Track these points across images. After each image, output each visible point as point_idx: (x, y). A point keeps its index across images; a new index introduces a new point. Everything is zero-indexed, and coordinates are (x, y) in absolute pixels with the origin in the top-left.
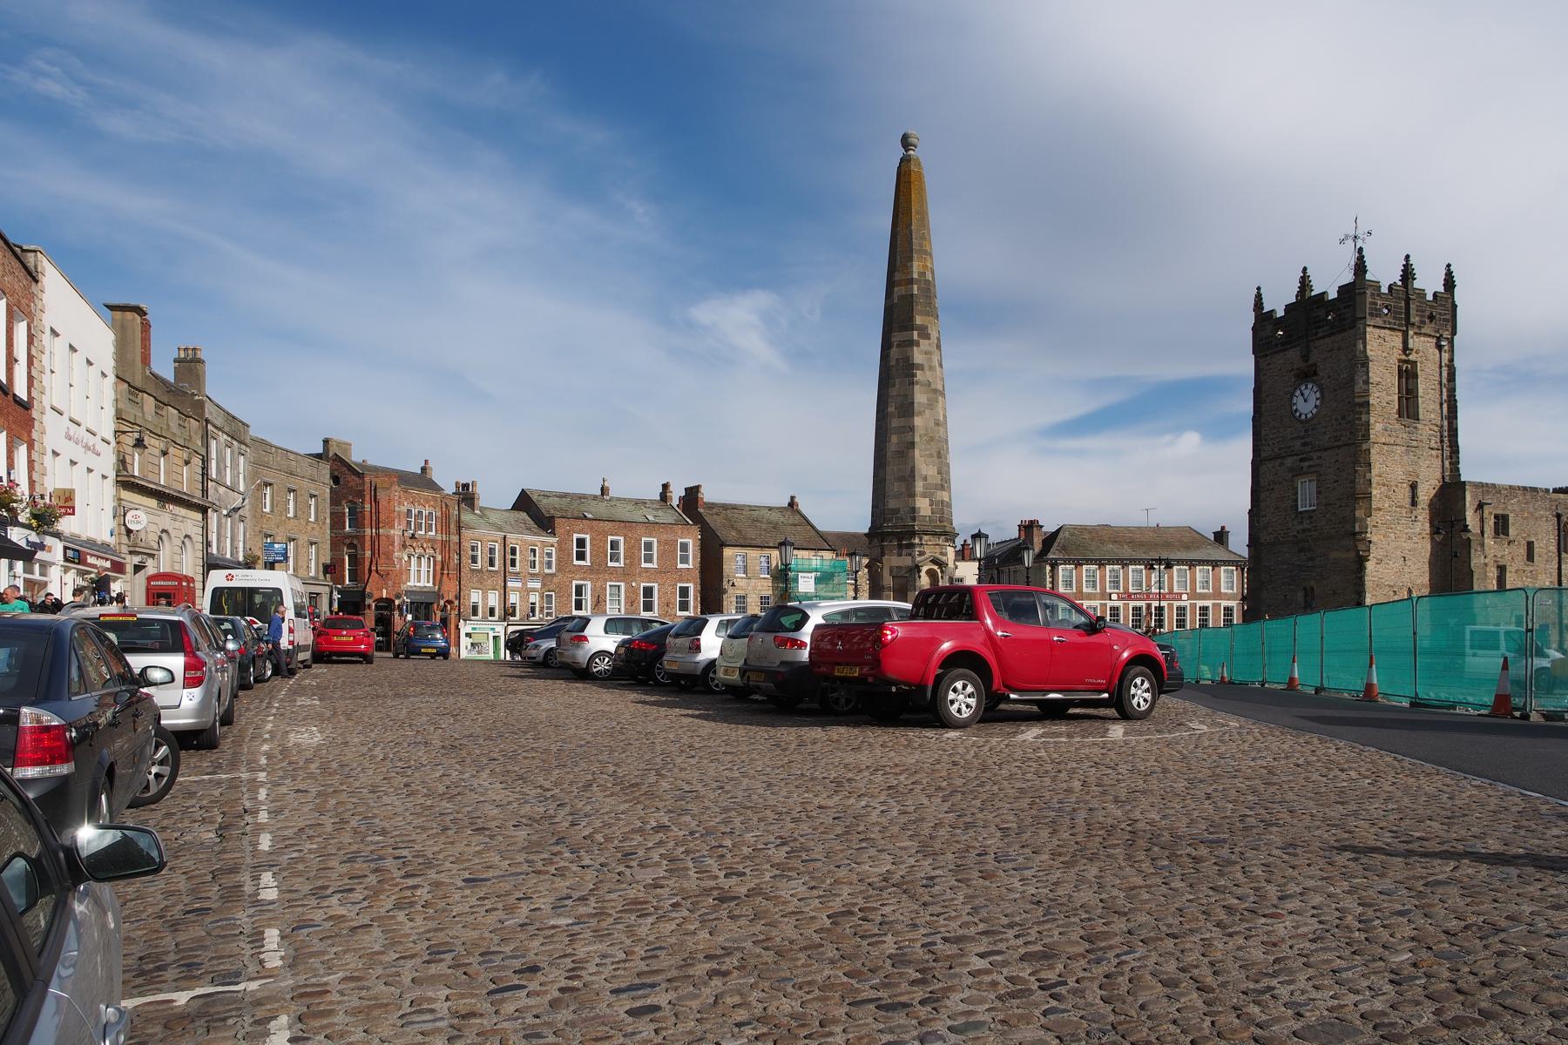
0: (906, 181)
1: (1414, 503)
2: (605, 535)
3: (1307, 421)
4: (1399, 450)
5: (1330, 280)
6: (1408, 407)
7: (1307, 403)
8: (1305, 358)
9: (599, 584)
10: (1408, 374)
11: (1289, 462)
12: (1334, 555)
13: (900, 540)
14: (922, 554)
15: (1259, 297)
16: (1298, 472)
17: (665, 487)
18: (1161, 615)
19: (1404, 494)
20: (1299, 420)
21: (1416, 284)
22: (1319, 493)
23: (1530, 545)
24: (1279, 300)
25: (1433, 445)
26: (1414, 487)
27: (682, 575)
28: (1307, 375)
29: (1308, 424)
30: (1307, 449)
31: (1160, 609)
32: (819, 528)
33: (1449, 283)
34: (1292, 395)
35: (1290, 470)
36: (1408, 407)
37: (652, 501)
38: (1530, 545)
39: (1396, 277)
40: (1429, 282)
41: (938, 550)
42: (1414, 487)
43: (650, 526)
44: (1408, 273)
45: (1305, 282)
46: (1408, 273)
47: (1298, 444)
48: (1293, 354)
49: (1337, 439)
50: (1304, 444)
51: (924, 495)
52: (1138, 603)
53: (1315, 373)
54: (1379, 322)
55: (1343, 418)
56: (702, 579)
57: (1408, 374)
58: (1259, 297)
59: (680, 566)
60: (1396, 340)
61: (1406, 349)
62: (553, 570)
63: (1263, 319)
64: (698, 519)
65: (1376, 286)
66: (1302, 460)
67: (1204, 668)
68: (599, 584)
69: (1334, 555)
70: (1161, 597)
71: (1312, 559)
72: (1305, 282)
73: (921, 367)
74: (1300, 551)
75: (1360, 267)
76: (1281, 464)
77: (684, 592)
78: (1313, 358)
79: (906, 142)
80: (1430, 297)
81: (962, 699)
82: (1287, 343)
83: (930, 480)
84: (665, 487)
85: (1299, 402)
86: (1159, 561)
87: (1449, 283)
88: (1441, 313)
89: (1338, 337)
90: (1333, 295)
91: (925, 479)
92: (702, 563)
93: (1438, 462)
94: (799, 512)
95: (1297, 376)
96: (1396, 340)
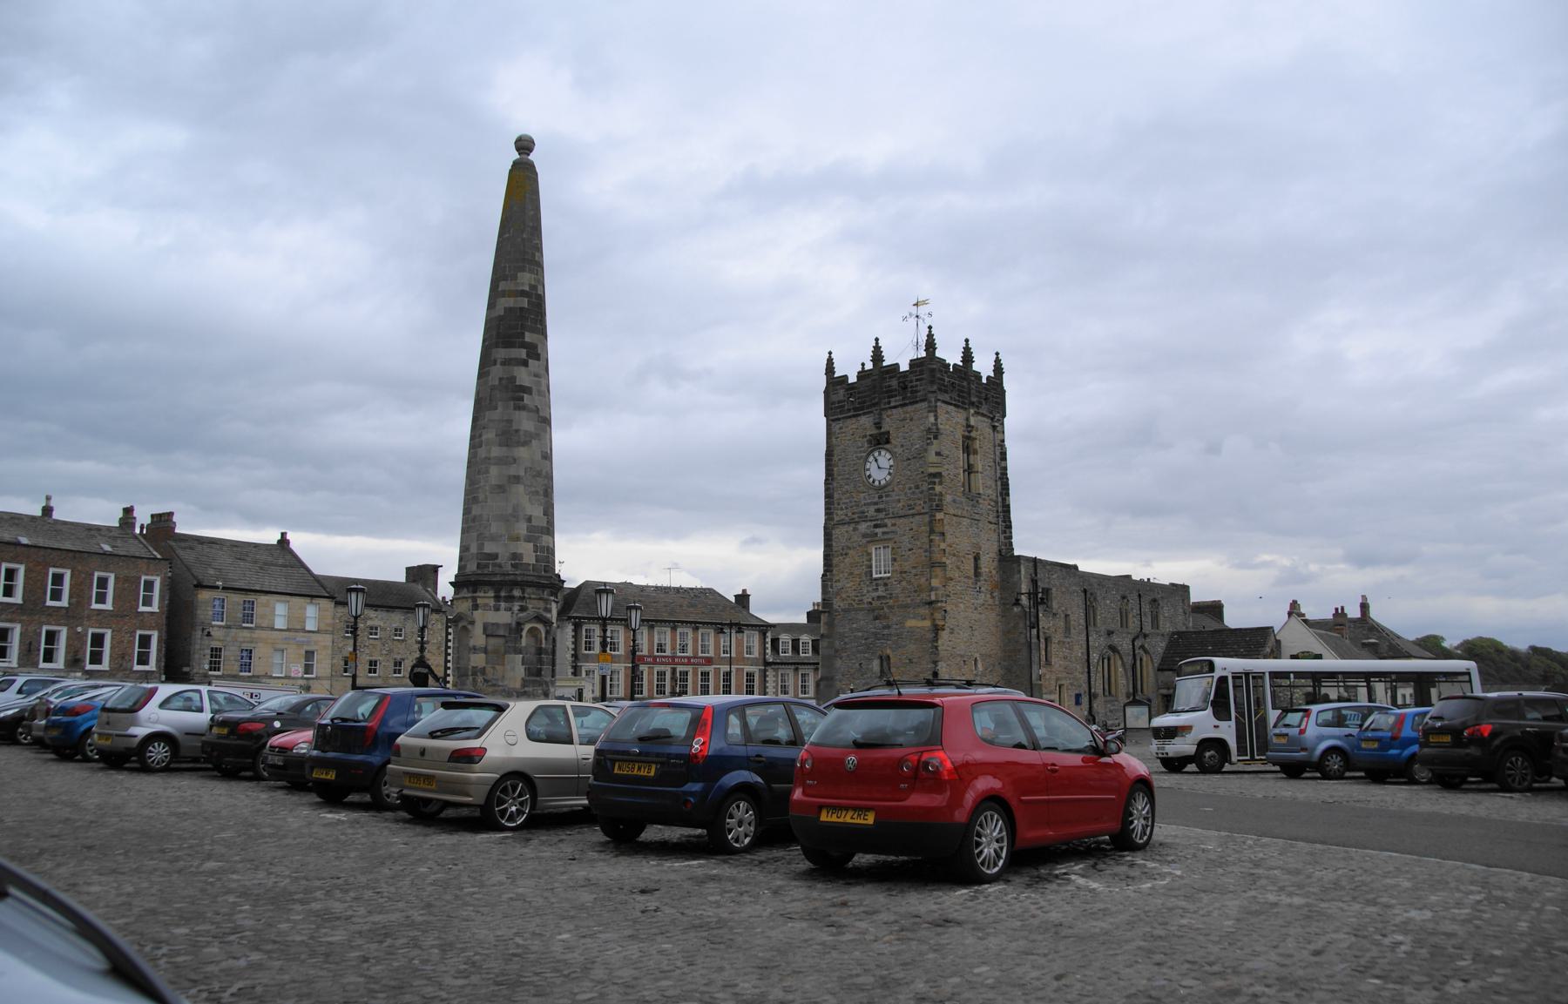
0: (523, 183)
1: (977, 574)
2: (47, 566)
3: (881, 488)
4: (966, 522)
5: (901, 355)
7: (880, 468)
8: (878, 425)
9: (32, 628)
11: (863, 527)
12: (910, 623)
13: (497, 591)
14: (523, 609)
15: (830, 362)
16: (872, 538)
18: (804, 687)
19: (969, 566)
22: (894, 560)
24: (849, 369)
25: (991, 518)
26: (977, 558)
28: (880, 440)
29: (882, 490)
30: (882, 515)
31: (728, 675)
32: (316, 571)
33: (998, 369)
34: (866, 460)
35: (865, 536)
37: (109, 529)
40: (983, 366)
41: (541, 604)
42: (977, 558)
43: (107, 559)
44: (968, 356)
45: (877, 355)
46: (968, 356)
47: (871, 511)
48: (866, 421)
49: (911, 507)
50: (878, 511)
51: (528, 540)
52: (662, 668)
53: (888, 442)
54: (946, 397)
55: (917, 487)
56: (168, 625)
58: (830, 362)
59: (142, 609)
63: (834, 383)
64: (169, 559)
65: (978, 375)
66: (876, 526)
68: (32, 628)
69: (910, 623)
70: (709, 661)
71: (888, 627)
72: (877, 355)
73: (528, 390)
74: (876, 618)
75: (931, 345)
76: (855, 529)
77: (145, 641)
81: (991, 841)
82: (858, 410)
83: (534, 523)
84: (128, 511)
85: (872, 467)
86: (731, 625)
87: (998, 369)
89: (910, 408)
90: (904, 367)
91: (529, 519)
93: (995, 536)
94: (292, 553)
95: (869, 442)
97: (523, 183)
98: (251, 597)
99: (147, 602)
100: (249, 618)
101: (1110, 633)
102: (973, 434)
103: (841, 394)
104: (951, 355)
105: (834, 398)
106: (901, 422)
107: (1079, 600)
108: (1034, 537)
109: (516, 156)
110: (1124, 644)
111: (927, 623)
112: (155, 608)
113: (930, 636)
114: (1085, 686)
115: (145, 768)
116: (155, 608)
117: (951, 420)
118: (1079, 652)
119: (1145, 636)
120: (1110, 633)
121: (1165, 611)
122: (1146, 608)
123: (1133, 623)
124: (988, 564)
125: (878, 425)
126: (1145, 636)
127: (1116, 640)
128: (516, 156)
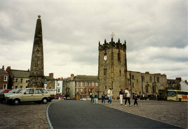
0: (39, 22)
3: (106, 61)
6: (119, 58)
8: (105, 52)
10: (119, 54)
17: (3, 66)
20: (104, 61)
21: (120, 43)
23: (137, 80)
24: (102, 43)
26: (120, 72)
27: (5, 82)
28: (105, 54)
29: (106, 61)
33: (125, 43)
36: (119, 58)
38: (137, 80)
39: (117, 42)
40: (122, 42)
44: (119, 41)
46: (119, 41)
48: (104, 51)
57: (119, 54)
59: (4, 81)
60: (118, 50)
61: (119, 51)
62: (5, 76)
65: (121, 44)
67: (109, 91)
74: (105, 80)
78: (106, 52)
79: (39, 17)
80: (122, 44)
82: (103, 50)
84: (3, 66)
87: (125, 43)
88: (124, 47)
92: (9, 80)
96: (118, 50)
97: (39, 22)
98: (18, 78)
99: (5, 80)
100: (21, 82)
101: (147, 83)
102: (120, 53)
103: (101, 48)
104: (116, 41)
105: (100, 48)
106: (109, 52)
107: (141, 77)
108: (131, 67)
109: (38, 18)
110: (151, 84)
111: (111, 81)
112: (6, 81)
113: (111, 83)
114: (142, 91)
115: (43, 103)
116: (6, 81)
117: (116, 51)
118: (140, 85)
119: (156, 83)
120: (147, 83)
121: (160, 79)
122: (156, 79)
123: (153, 81)
124: (123, 72)
125: (105, 52)
126: (156, 83)
127: (149, 84)
128: (38, 18)
